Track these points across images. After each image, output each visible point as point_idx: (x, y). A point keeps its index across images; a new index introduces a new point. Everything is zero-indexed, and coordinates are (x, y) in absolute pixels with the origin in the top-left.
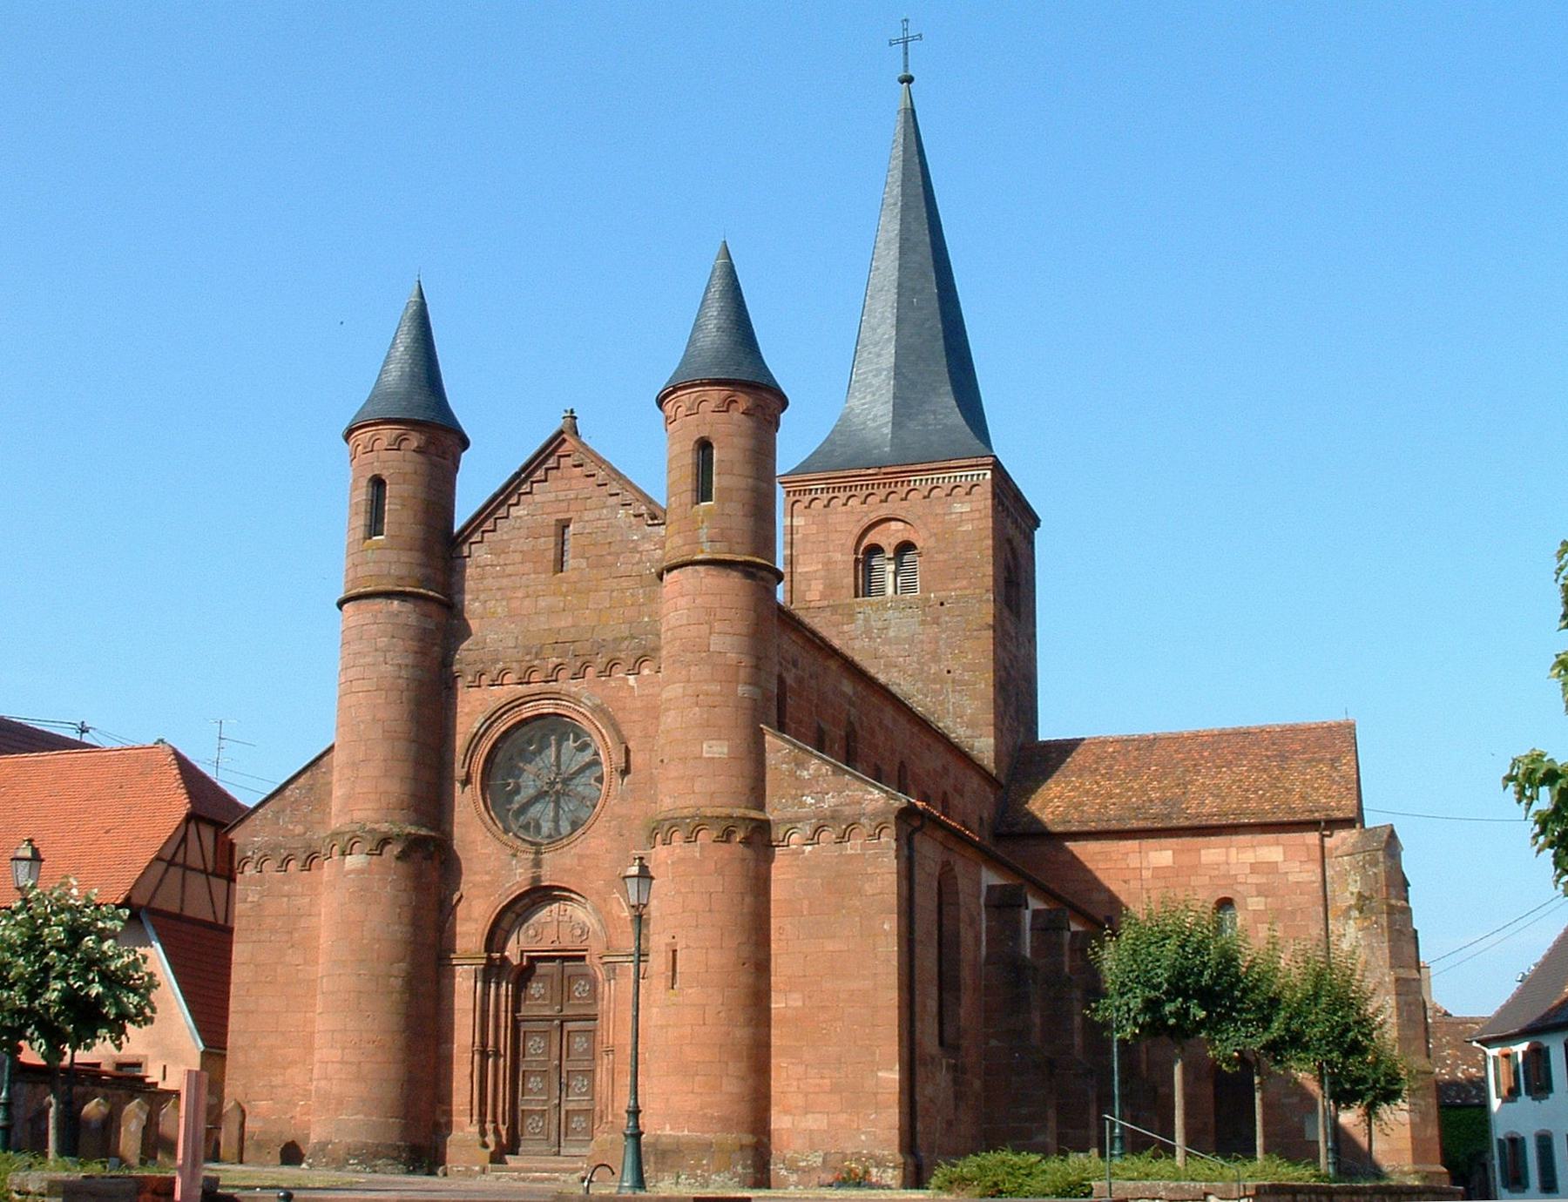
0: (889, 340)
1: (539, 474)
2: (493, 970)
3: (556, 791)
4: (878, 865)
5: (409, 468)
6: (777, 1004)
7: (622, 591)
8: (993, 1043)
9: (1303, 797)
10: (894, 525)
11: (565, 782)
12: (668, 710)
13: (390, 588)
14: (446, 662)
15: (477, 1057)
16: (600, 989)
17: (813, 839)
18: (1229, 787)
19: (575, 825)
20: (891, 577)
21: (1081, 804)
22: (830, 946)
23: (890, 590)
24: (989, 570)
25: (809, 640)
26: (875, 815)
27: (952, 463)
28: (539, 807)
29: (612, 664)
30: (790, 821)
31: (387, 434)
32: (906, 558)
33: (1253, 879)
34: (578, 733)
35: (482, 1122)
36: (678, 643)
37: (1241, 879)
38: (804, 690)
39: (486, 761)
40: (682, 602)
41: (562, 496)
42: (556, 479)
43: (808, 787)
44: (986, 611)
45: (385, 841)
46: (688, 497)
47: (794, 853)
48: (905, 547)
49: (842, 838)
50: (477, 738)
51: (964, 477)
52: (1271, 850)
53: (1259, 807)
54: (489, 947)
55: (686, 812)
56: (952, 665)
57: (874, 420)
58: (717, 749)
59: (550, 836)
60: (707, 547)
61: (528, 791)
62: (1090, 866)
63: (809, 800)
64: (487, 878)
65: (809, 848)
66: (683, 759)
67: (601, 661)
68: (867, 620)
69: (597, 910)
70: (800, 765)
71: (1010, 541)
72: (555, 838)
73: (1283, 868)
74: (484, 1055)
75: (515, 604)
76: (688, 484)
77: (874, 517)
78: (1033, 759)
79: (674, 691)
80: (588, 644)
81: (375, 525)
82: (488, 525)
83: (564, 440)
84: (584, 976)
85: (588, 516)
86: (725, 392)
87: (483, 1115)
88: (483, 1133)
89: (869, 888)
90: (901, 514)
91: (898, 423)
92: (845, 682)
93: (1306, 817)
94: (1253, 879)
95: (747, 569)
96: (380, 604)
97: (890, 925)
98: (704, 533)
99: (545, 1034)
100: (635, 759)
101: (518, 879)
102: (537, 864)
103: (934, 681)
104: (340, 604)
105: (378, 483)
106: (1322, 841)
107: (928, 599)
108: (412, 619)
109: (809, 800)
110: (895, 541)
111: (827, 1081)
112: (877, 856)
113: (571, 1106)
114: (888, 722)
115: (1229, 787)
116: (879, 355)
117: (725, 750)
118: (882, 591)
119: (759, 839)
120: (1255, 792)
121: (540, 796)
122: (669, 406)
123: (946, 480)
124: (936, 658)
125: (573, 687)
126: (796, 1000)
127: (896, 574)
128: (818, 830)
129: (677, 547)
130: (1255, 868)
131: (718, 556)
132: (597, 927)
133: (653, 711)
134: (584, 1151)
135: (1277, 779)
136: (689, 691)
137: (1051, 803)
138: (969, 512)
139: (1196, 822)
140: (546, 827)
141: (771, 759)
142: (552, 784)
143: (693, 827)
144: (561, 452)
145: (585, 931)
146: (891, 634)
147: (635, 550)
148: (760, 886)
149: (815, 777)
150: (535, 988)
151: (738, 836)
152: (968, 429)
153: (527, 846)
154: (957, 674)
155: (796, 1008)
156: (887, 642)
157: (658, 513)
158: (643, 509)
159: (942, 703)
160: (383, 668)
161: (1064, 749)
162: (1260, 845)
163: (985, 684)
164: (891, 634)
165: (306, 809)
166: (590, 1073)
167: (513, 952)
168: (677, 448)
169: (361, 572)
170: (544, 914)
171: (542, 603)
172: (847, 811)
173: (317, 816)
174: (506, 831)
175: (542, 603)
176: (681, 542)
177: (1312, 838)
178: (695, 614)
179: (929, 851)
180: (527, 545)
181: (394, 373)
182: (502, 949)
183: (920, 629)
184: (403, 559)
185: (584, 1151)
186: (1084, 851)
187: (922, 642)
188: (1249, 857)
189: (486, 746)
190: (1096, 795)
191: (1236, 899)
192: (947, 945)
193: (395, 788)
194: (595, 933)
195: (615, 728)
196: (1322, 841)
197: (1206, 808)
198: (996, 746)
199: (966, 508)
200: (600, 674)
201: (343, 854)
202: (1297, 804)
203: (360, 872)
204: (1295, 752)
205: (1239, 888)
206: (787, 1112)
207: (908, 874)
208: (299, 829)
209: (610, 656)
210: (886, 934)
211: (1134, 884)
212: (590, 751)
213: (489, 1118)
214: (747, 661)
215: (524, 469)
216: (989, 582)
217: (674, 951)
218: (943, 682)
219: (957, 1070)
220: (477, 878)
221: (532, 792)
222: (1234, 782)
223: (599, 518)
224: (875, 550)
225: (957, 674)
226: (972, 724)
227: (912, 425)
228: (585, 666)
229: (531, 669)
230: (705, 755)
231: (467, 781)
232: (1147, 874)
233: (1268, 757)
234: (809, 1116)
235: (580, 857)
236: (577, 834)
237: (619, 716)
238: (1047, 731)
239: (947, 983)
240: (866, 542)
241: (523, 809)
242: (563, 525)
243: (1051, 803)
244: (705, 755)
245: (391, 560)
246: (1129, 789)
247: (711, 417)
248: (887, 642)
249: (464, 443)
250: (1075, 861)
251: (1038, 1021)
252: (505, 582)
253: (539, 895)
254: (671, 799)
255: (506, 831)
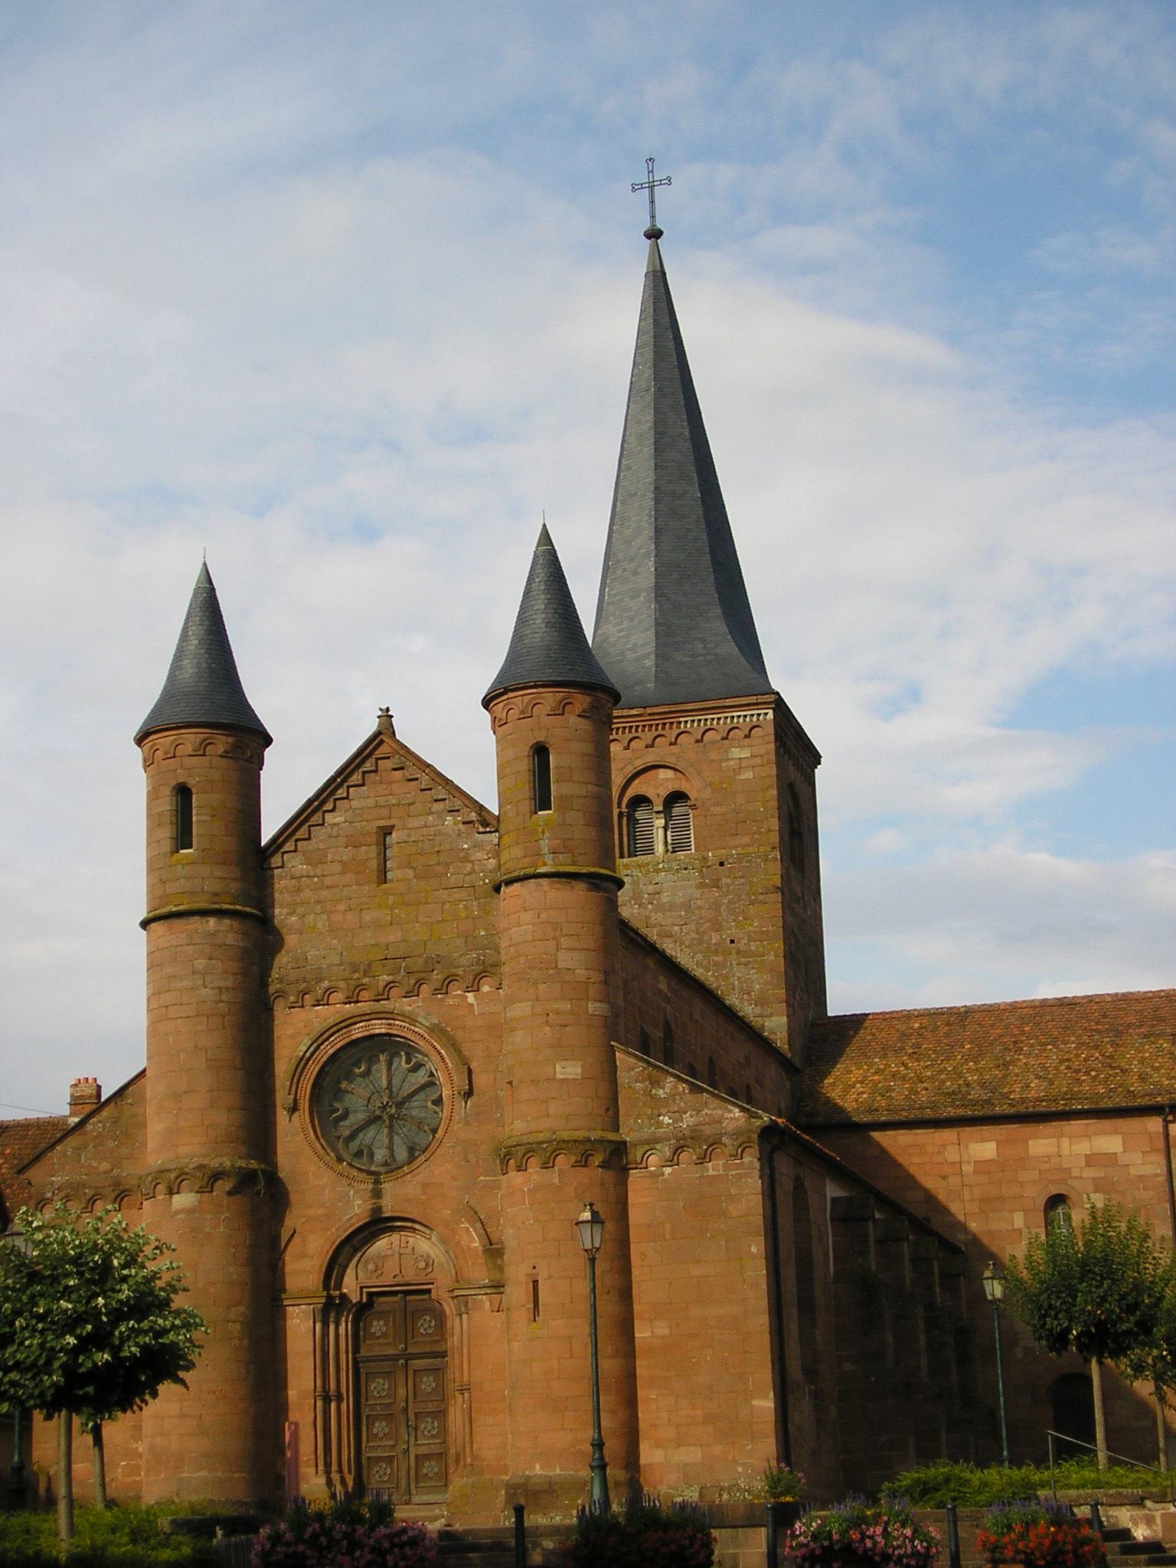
0: (647, 555)
1: (356, 778)
2: (332, 1307)
3: (390, 1112)
4: (741, 1184)
5: (216, 775)
6: (641, 1333)
7: (456, 902)
8: (847, 1366)
9: (1143, 1078)
10: (663, 774)
11: (399, 1105)
12: (513, 1030)
13: (204, 905)
14: (263, 983)
15: (319, 1403)
16: (449, 1324)
17: (671, 1162)
18: (1056, 1068)
19: (412, 1152)
20: (661, 832)
21: (889, 1089)
22: (697, 1271)
23: (660, 848)
24: (775, 823)
25: (632, 940)
26: (736, 1134)
27: (728, 702)
28: (371, 1132)
29: (449, 980)
30: (647, 1142)
31: (190, 739)
32: (676, 811)
33: (1091, 1173)
34: (410, 1049)
35: (328, 1472)
36: (522, 960)
37: (1075, 1173)
38: (653, 1007)
39: (314, 1085)
40: (526, 917)
41: (382, 801)
42: (374, 783)
43: (667, 1108)
44: (772, 872)
45: (217, 1176)
46: (526, 806)
47: (653, 1175)
48: (676, 797)
49: (702, 1159)
50: (303, 1062)
51: (742, 717)
52: (1108, 1140)
53: (1092, 1089)
54: (326, 1286)
55: (541, 1137)
56: (735, 933)
57: (633, 649)
58: (570, 1070)
59: (386, 1164)
60: (549, 859)
61: (358, 1117)
62: (901, 1160)
63: (666, 1120)
64: (321, 1211)
65: (667, 1170)
66: (535, 1082)
67: (437, 977)
68: (635, 883)
69: (444, 1241)
70: (655, 1083)
71: (791, 785)
72: (392, 1167)
73: (1123, 1160)
74: (327, 1399)
75: (336, 918)
76: (524, 790)
77: (639, 764)
78: (828, 1037)
79: (521, 1009)
80: (421, 961)
81: (183, 838)
82: (302, 833)
83: (382, 741)
84: (428, 1310)
85: (413, 823)
86: (560, 693)
87: (328, 1465)
88: (329, 1483)
89: (734, 1210)
90: (670, 760)
91: (662, 653)
92: (661, 978)
93: (1146, 1101)
94: (1091, 1173)
95: (593, 880)
96: (195, 923)
97: (757, 1247)
98: (545, 845)
99: (388, 1375)
100: (481, 1080)
101: (358, 1210)
102: (377, 1194)
103: (716, 953)
104: (145, 924)
105: (183, 793)
106: (1166, 1128)
107: (705, 859)
108: (231, 939)
109: (666, 1120)
110: (664, 793)
111: (699, 1412)
112: (739, 1177)
113: (422, 1450)
114: (697, 1016)
115: (1056, 1068)
116: (636, 573)
117: (579, 1070)
118: (650, 850)
119: (617, 1159)
120: (1087, 1073)
121: (374, 1120)
122: (499, 708)
123: (720, 721)
124: (717, 927)
125: (406, 1005)
126: (662, 1329)
127: (666, 829)
128: (677, 1150)
129: (514, 858)
130: (1091, 1160)
131: (562, 869)
132: (443, 1259)
133: (497, 1030)
134: (438, 1498)
135: (1111, 1057)
136: (538, 1010)
137: (849, 1086)
138: (751, 758)
139: (1022, 1109)
140: (380, 1155)
141: (623, 1078)
142: (384, 1107)
143: (548, 1152)
144: (378, 753)
145: (429, 1263)
146: (665, 898)
147: (466, 859)
148: (614, 1214)
149: (672, 1096)
150: (377, 1327)
151: (597, 1159)
152: (742, 660)
153: (364, 1175)
154: (742, 945)
155: (663, 1337)
156: (660, 908)
157: (488, 818)
158: (473, 816)
159: (726, 977)
160: (203, 991)
161: (856, 1021)
162: (1096, 1134)
163: (774, 954)
164: (665, 898)
165: (111, 1144)
166: (441, 1414)
167: (350, 1286)
168: (510, 754)
169: (171, 888)
170: (381, 1245)
171: (367, 917)
172: (708, 1130)
173: (124, 1151)
174: (340, 1160)
175: (367, 917)
176: (520, 854)
177: (1155, 1124)
178: (537, 923)
179: (785, 1167)
180: (347, 854)
181: (189, 670)
182: (339, 1286)
183: (697, 893)
184: (219, 874)
185: (438, 1498)
186: (895, 1142)
187: (700, 908)
188: (1083, 1147)
189: (313, 1069)
190: (904, 1078)
191: (1072, 1196)
192: (805, 1265)
193: (223, 1119)
194: (440, 1264)
195: (455, 1047)
196: (1166, 1128)
197: (1034, 1091)
198: (789, 1026)
199: (745, 753)
200: (436, 991)
201: (171, 1192)
202: (1136, 1086)
203: (190, 1211)
204: (1129, 1026)
205: (1075, 1183)
206: (658, 1444)
207: (770, 1194)
208: (105, 1166)
209: (447, 972)
210: (754, 1257)
211: (954, 1181)
212: (422, 1072)
213: (334, 1467)
214: (597, 977)
215: (339, 773)
216: (775, 837)
217: (535, 1282)
218: (726, 953)
219: (816, 1395)
220: (312, 1212)
221: (361, 1116)
222: (1062, 1061)
223: (422, 825)
224: (640, 801)
225: (742, 945)
226: (761, 1002)
227: (678, 656)
228: (420, 983)
229: (361, 987)
230: (559, 1076)
231: (294, 1109)
232: (967, 1169)
233: (1099, 1032)
234: (682, 1449)
235: (425, 1186)
236: (417, 1162)
237: (460, 1035)
238: (840, 1000)
239: (806, 1305)
240: (630, 793)
241: (352, 1136)
242: (387, 831)
243: (849, 1086)
244: (559, 1076)
245: (204, 875)
246: (941, 1072)
247: (545, 719)
248: (660, 908)
249: (268, 741)
250: (884, 1157)
251: (890, 1340)
252: (324, 894)
253: (377, 1225)
254: (521, 1123)
255: (340, 1160)
